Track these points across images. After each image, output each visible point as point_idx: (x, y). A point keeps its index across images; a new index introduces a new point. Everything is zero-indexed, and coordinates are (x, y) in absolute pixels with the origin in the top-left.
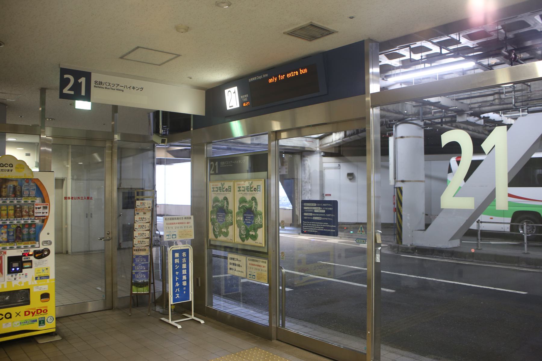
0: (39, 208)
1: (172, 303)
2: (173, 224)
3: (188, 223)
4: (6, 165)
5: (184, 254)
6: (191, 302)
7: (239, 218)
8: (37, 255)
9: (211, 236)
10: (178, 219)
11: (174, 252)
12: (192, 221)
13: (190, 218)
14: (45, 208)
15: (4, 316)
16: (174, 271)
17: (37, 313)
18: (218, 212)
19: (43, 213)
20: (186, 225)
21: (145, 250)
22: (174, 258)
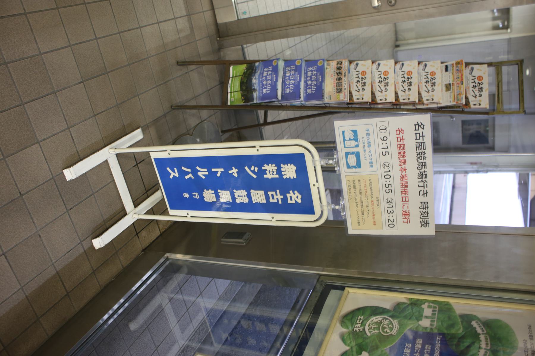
1: (153, 156)
2: (402, 154)
3: (406, 214)
5: (294, 197)
6: (168, 214)
7: (427, 311)
9: (357, 297)
10: (423, 176)
11: (298, 160)
12: (412, 229)
13: (425, 224)
16: (240, 162)
18: (445, 339)
20: (399, 209)
21: (339, 91)
22: (279, 160)
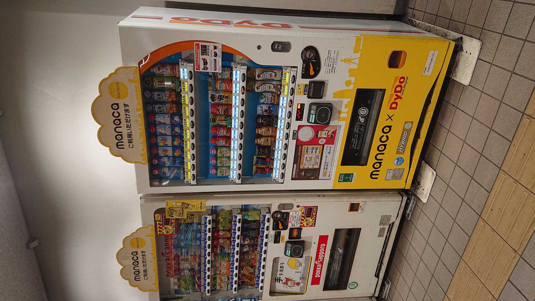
0: (205, 63)
4: (116, 114)
8: (312, 73)
14: (205, 50)
15: (116, 111)
17: (400, 92)
19: (216, 55)
